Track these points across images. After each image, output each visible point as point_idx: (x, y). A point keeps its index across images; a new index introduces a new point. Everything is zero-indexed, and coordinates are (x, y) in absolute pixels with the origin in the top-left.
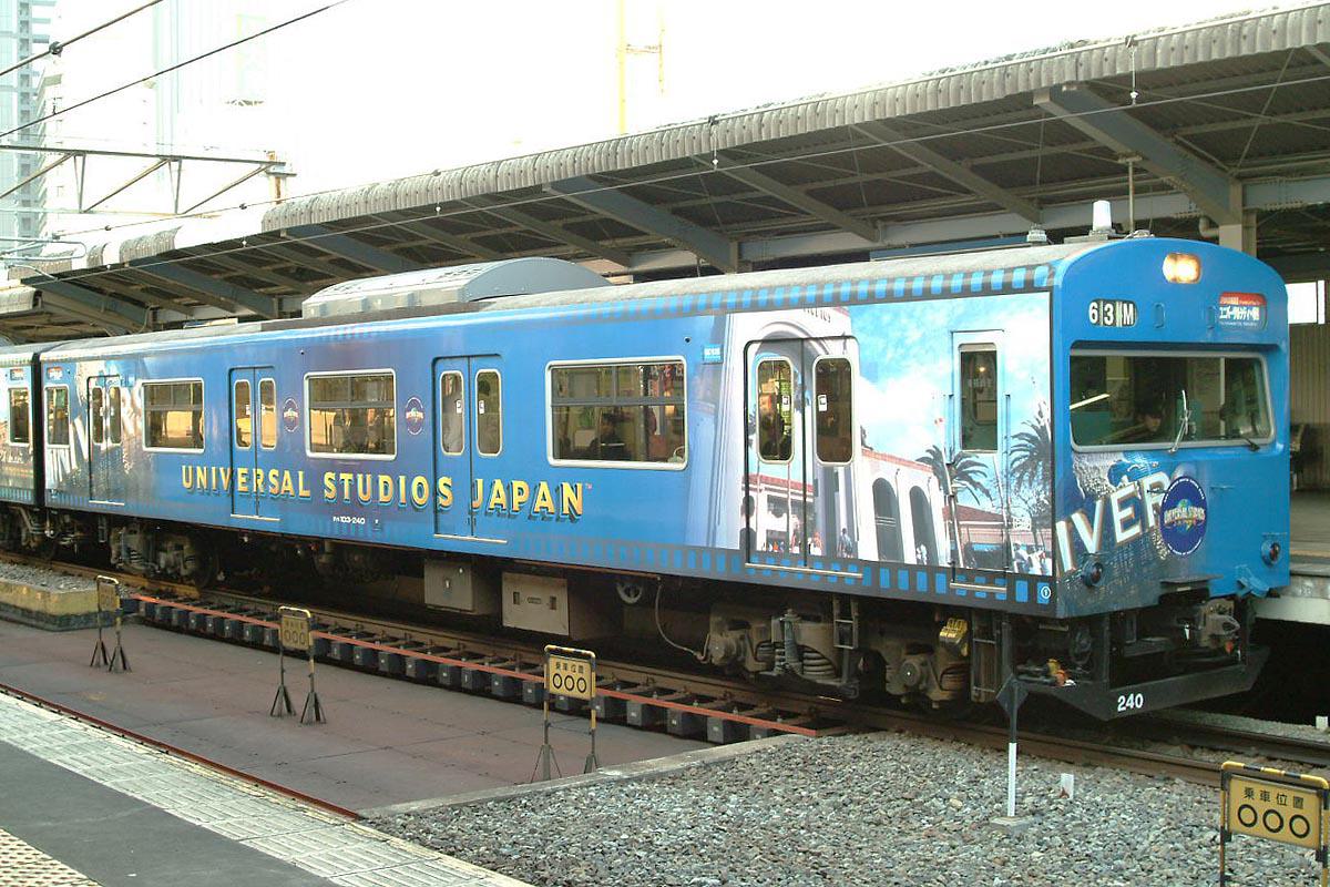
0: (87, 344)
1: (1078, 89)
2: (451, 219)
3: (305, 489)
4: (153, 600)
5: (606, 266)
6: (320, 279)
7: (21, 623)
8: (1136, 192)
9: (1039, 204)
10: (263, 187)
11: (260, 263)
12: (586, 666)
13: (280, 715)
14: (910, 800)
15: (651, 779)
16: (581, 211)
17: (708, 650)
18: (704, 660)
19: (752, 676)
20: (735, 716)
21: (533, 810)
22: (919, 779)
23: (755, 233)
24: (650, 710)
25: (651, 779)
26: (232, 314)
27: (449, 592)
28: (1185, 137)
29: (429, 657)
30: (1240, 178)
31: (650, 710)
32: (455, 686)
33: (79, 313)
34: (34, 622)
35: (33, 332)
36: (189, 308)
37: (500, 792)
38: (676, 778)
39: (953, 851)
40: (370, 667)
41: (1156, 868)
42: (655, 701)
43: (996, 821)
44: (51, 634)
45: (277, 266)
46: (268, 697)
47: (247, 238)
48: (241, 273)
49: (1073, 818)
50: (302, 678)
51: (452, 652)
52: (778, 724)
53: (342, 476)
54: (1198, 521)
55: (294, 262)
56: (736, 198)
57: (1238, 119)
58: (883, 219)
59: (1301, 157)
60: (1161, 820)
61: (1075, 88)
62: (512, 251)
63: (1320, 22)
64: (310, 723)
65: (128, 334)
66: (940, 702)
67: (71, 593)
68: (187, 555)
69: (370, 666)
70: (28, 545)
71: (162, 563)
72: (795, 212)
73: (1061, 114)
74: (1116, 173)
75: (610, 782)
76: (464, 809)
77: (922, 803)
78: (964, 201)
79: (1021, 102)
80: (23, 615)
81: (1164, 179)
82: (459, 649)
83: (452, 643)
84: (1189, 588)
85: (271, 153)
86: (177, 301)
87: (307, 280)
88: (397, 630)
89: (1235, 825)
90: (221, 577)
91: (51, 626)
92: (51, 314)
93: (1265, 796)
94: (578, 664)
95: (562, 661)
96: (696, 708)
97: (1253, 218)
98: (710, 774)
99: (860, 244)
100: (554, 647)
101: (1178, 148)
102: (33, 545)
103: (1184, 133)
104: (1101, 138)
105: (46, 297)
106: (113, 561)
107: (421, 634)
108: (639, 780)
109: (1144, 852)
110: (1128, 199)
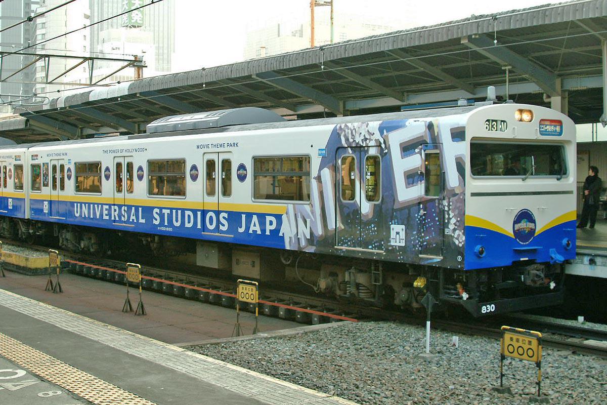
0: (309, 123)
1: (479, 36)
2: (214, 90)
4: (76, 262)
5: (285, 111)
6: (157, 115)
7: (15, 272)
8: (509, 82)
9: (474, 86)
10: (131, 72)
11: (129, 108)
12: (254, 288)
13: (126, 312)
14: (389, 347)
15: (280, 338)
16: (271, 87)
17: (319, 285)
18: (317, 290)
19: (338, 297)
20: (325, 314)
21: (226, 348)
22: (395, 339)
23: (350, 97)
24: (288, 311)
25: (280, 338)
26: (116, 131)
27: (208, 260)
28: (532, 57)
29: (196, 288)
30: (560, 75)
31: (288, 311)
32: (206, 301)
33: (47, 130)
34: (21, 272)
35: (24, 138)
36: (97, 128)
37: (214, 341)
38: (290, 338)
39: (399, 366)
40: (169, 292)
41: (483, 374)
42: (291, 307)
43: (421, 355)
44: (28, 277)
45: (136, 109)
46: (120, 304)
47: (121, 97)
48: (120, 112)
49: (455, 355)
50: (136, 296)
51: (206, 286)
52: (343, 317)
54: (531, 229)
55: (143, 108)
56: (340, 82)
57: (384, 73)
58: (408, 92)
59: (495, 77)
60: (492, 355)
61: (477, 37)
62: (241, 104)
63: (577, 10)
64: (139, 315)
65: (69, 140)
66: (417, 309)
67: (39, 259)
68: (92, 242)
69: (169, 292)
70: (22, 237)
71: (82, 246)
72: (365, 88)
73: (475, 48)
74: (501, 73)
75: (261, 339)
76: (196, 347)
77: (393, 349)
78: (438, 84)
79: (456, 41)
80: (17, 269)
81: (524, 76)
82: (289, 301)
83: (319, 304)
85: (136, 57)
86: (91, 124)
87: (150, 116)
88: (183, 276)
89: (506, 353)
90: (109, 253)
91: (30, 274)
92: (34, 130)
93: (518, 340)
94: (251, 288)
95: (244, 286)
96: (308, 310)
97: (567, 94)
98: (306, 336)
99: (396, 102)
100: (242, 280)
101: (530, 62)
102: (24, 237)
103: (533, 56)
104: (493, 58)
105: (31, 122)
106: (60, 245)
107: (193, 278)
108: (275, 338)
109: (480, 368)
110: (506, 85)
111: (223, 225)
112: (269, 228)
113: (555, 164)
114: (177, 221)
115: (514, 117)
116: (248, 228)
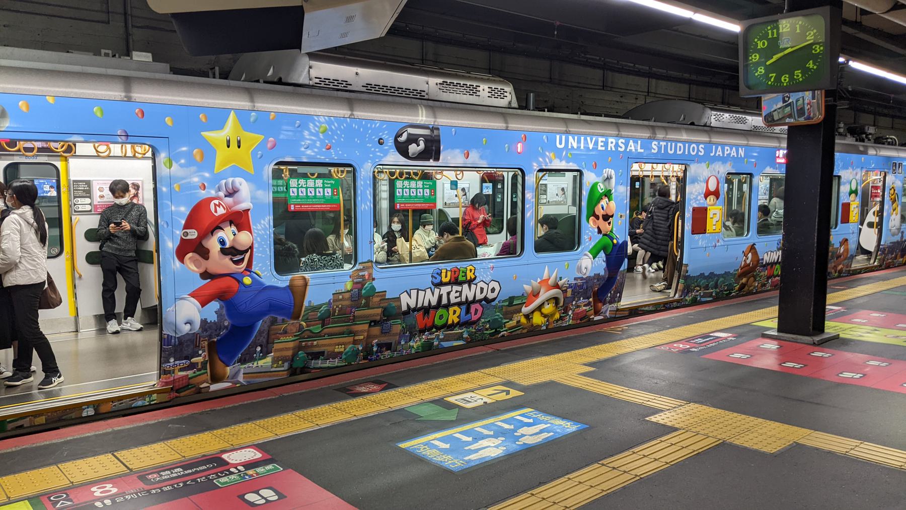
3: (641, 149)
53: (661, 143)
84: (900, 325)
111: (701, 152)
112: (726, 153)
113: (636, 234)
114: (671, 150)
115: (250, 120)
116: (716, 153)
